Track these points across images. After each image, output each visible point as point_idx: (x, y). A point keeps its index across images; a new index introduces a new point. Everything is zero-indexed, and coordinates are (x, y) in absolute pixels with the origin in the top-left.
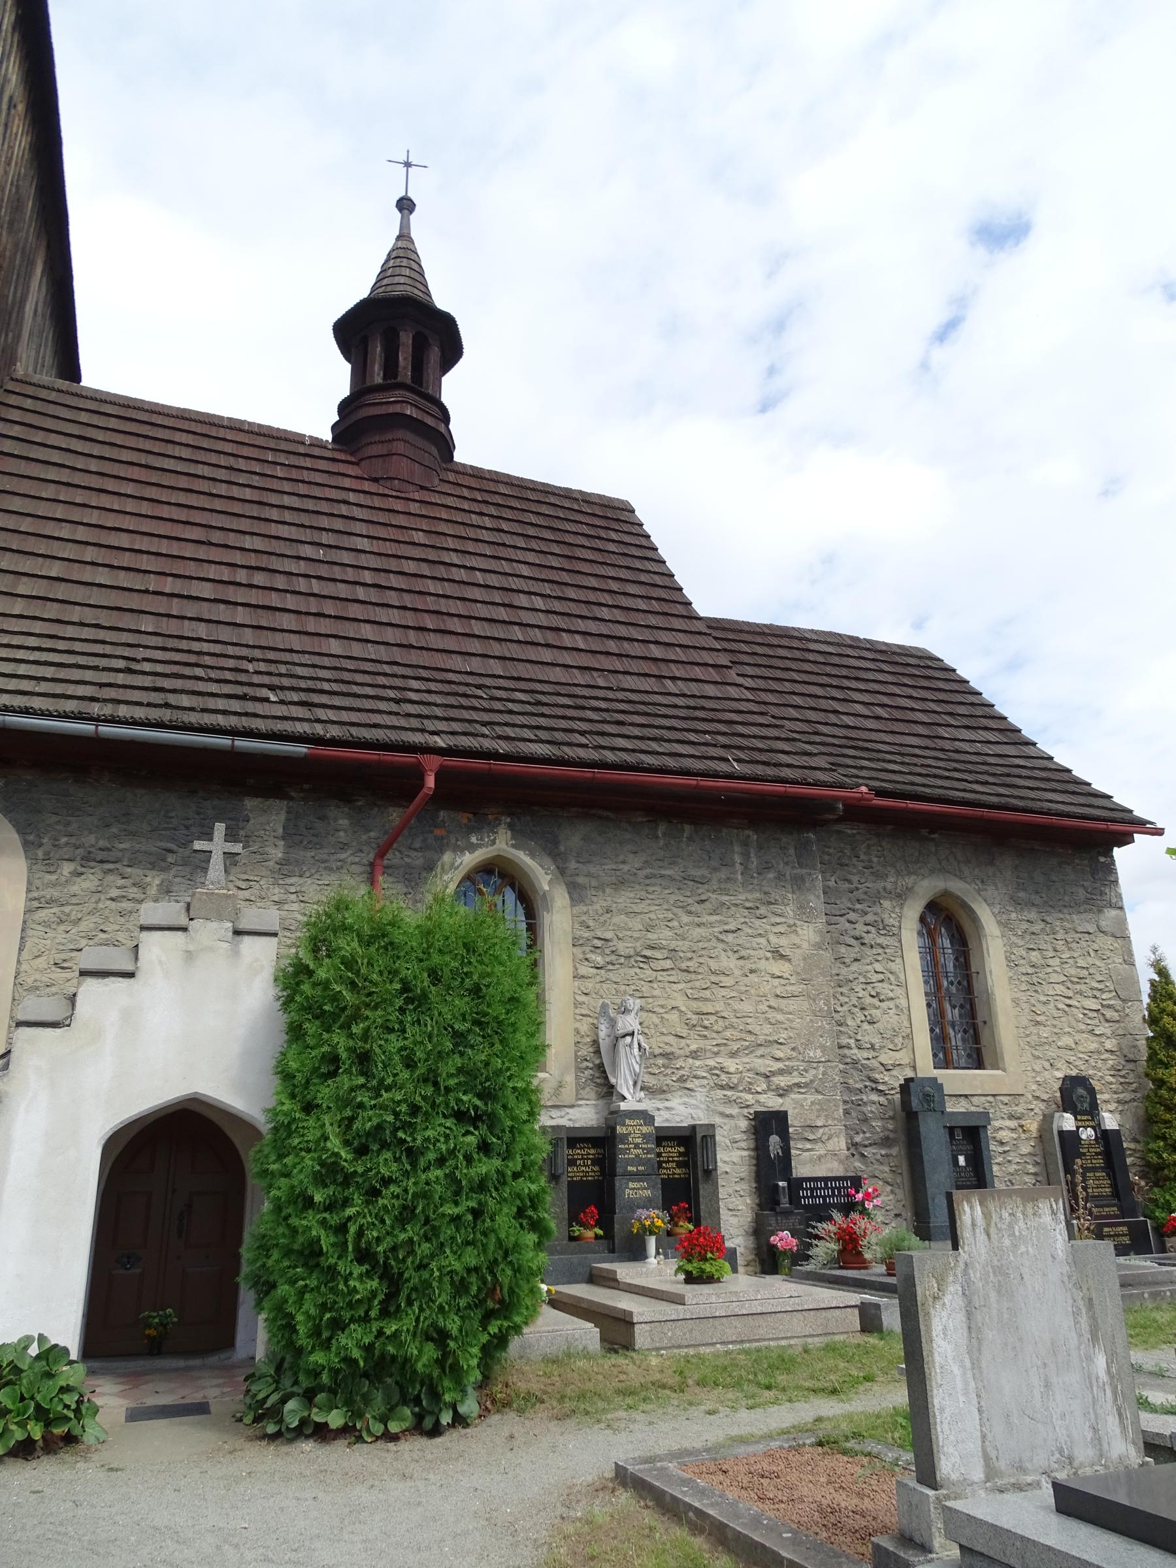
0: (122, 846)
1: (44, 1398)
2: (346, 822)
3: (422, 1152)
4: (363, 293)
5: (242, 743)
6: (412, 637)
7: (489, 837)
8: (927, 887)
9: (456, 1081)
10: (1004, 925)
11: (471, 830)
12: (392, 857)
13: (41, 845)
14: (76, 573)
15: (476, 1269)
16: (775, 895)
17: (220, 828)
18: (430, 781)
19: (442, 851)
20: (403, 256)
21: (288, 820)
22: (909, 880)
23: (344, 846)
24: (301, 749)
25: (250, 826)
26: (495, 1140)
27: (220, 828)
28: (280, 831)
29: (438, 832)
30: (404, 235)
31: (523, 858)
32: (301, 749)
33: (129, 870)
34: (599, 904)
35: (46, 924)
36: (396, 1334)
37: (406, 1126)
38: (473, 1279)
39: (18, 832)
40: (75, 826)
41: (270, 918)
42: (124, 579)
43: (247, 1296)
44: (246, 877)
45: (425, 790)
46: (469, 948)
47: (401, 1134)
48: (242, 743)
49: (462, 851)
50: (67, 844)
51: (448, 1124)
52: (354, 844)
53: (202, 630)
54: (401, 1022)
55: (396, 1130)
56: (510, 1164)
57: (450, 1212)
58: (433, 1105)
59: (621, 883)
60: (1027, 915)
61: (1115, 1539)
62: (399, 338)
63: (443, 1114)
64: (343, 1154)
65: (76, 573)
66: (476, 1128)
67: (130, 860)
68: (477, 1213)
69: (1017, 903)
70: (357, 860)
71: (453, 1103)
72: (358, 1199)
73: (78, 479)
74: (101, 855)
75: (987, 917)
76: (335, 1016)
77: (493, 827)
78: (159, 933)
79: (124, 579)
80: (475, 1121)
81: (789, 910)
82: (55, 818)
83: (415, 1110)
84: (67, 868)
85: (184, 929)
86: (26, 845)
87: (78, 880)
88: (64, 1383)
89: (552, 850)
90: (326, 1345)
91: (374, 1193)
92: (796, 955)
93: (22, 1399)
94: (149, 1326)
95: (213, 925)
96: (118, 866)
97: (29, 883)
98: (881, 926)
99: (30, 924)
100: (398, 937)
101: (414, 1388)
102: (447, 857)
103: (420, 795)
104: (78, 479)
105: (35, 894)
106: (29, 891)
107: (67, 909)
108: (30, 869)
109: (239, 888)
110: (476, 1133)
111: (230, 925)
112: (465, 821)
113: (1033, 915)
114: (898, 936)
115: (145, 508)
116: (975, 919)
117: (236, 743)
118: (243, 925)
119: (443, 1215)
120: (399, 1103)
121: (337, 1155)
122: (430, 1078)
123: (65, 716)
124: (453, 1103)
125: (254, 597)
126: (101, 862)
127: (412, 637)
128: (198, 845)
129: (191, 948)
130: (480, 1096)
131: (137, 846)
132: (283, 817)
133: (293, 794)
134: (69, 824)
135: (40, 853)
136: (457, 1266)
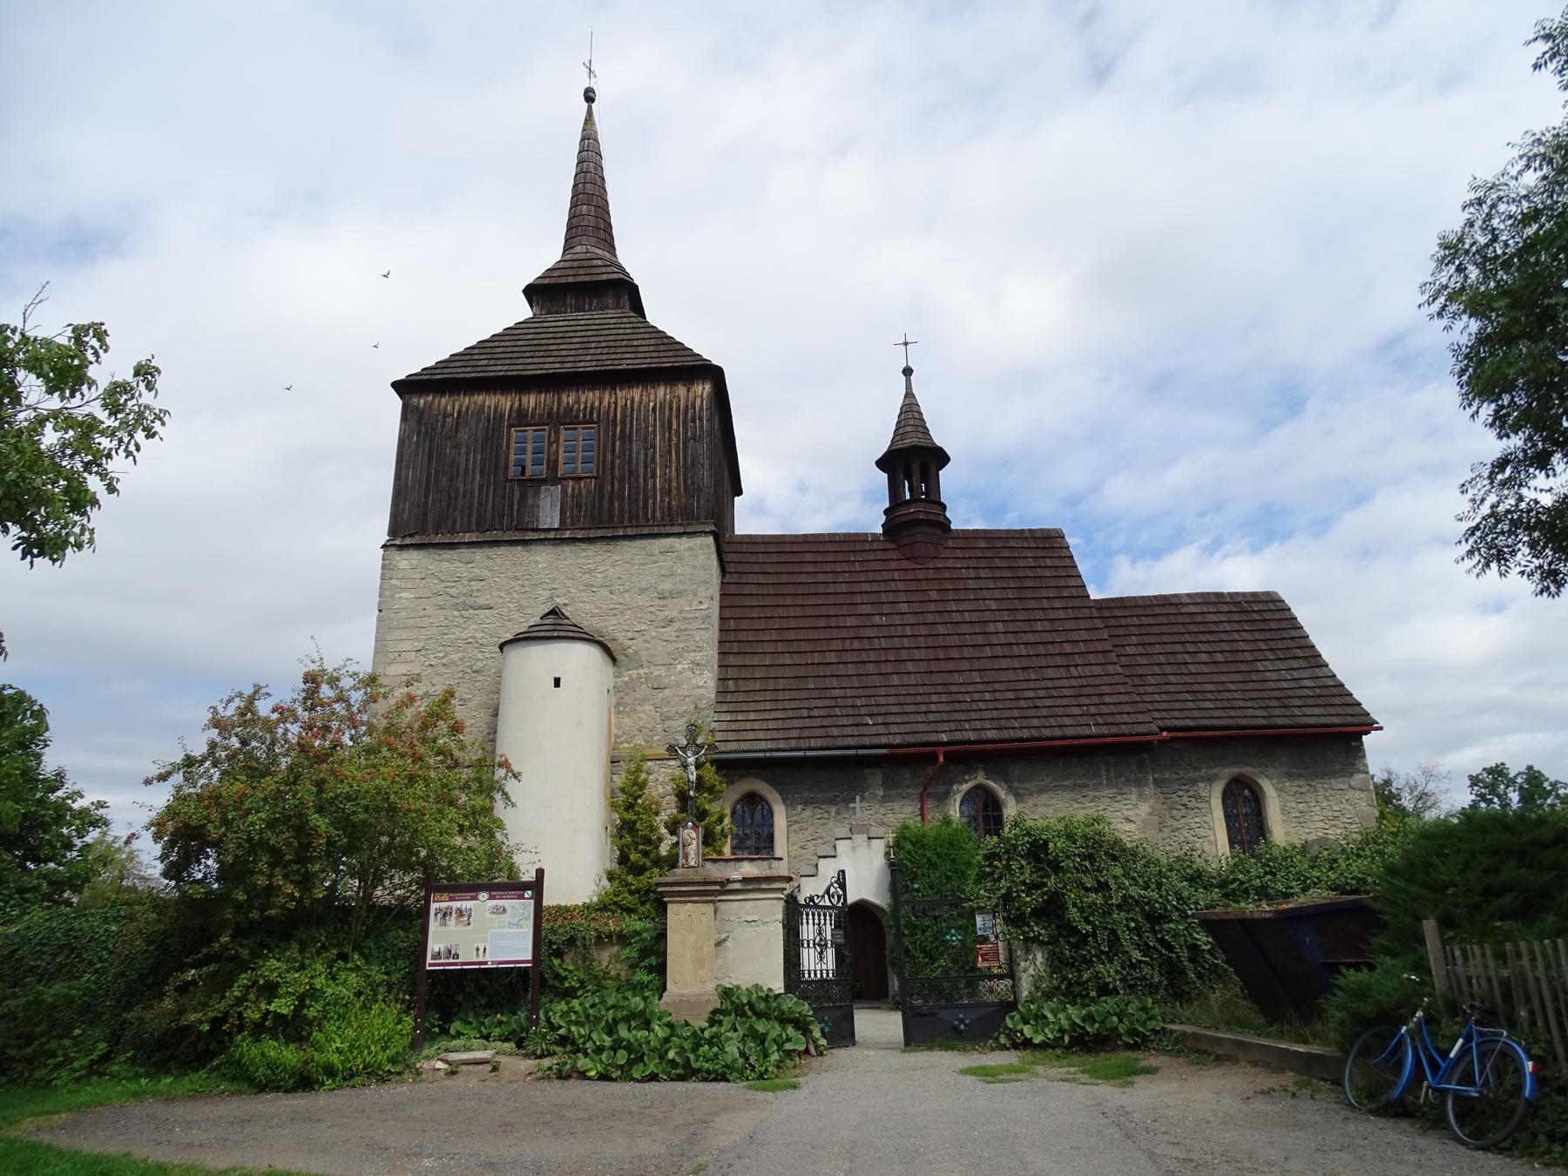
4: (885, 450)
5: (861, 752)
6: (933, 666)
8: (1228, 772)
10: (1280, 790)
11: (965, 773)
12: (931, 790)
16: (1125, 790)
18: (941, 759)
20: (910, 413)
22: (1216, 771)
24: (885, 751)
30: (909, 394)
31: (992, 784)
32: (885, 751)
34: (1031, 802)
41: (881, 831)
43: (889, 969)
46: (951, 844)
48: (861, 752)
59: (1041, 791)
60: (1297, 782)
61: (1391, 1136)
62: (913, 461)
69: (1290, 776)
75: (1269, 788)
77: (975, 771)
81: (1133, 797)
86: (784, 800)
89: (1004, 778)
91: (924, 932)
92: (1138, 820)
98: (1198, 797)
100: (925, 841)
113: (1301, 783)
114: (1208, 802)
116: (1261, 788)
123: (792, 750)
127: (933, 666)
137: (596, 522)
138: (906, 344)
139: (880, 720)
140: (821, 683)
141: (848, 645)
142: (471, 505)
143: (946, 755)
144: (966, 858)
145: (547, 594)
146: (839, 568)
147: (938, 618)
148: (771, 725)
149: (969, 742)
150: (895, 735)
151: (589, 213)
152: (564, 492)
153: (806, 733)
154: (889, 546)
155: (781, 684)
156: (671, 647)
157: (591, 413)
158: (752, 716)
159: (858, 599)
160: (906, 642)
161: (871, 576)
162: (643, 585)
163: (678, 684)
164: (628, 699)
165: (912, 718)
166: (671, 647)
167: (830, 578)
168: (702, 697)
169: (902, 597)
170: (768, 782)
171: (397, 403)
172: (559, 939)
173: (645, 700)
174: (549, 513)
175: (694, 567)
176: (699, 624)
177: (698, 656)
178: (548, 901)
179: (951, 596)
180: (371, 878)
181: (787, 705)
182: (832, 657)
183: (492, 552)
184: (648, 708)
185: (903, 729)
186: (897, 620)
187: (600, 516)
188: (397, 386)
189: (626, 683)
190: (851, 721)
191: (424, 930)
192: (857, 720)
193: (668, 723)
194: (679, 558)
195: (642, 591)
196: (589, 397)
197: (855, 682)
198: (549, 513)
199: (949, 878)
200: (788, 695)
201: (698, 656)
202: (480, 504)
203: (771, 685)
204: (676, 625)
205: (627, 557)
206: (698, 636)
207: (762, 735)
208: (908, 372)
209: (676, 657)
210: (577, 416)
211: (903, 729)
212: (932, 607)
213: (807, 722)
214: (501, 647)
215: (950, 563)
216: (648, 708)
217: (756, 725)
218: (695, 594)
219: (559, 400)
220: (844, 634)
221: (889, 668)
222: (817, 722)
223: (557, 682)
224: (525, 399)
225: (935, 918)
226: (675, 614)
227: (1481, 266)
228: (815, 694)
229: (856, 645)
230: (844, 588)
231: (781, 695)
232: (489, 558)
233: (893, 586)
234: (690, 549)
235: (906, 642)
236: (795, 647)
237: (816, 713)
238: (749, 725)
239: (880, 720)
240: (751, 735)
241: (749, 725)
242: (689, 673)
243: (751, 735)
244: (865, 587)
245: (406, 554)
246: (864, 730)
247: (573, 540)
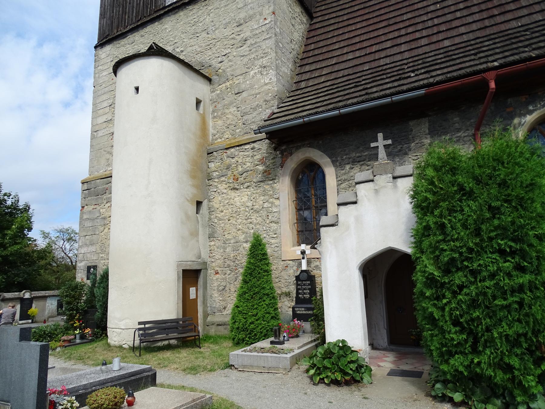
0: (365, 154)
1: (342, 365)
2: (458, 119)
3: (480, 272)
5: (395, 98)
7: (540, 104)
9: (495, 233)
11: (528, 103)
13: (337, 161)
14: (341, 59)
15: (525, 335)
17: (380, 136)
18: (493, 85)
19: (512, 118)
21: (429, 125)
23: (459, 130)
24: (422, 92)
25: (413, 133)
26: (526, 264)
27: (380, 136)
28: (427, 131)
29: (508, 110)
32: (422, 92)
33: (369, 162)
35: (345, 189)
36: (479, 363)
37: (467, 259)
38: (522, 339)
39: (330, 158)
40: (347, 151)
42: (358, 54)
44: (416, 154)
45: (490, 90)
47: (466, 263)
48: (395, 98)
49: (525, 115)
50: (346, 158)
51: (494, 257)
52: (464, 128)
53: (388, 60)
54: (461, 206)
55: (462, 261)
56: (539, 278)
57: (500, 303)
58: (482, 248)
63: (490, 251)
64: (436, 273)
65: (341, 59)
66: (513, 258)
67: (369, 158)
68: (521, 304)
70: (466, 134)
71: (495, 246)
72: (448, 295)
73: (340, 25)
74: (358, 159)
76: (427, 207)
78: (363, 184)
79: (358, 54)
80: (513, 253)
82: (340, 150)
83: (470, 250)
84: (348, 167)
85: (372, 181)
86: (334, 163)
87: (352, 170)
88: (349, 360)
90: (447, 362)
93: (333, 364)
94: (412, 335)
95: (384, 177)
96: (365, 162)
97: (337, 175)
99: (340, 190)
101: (499, 390)
102: (516, 121)
103: (489, 93)
104: (340, 25)
105: (339, 179)
106: (337, 178)
107: (351, 182)
108: (336, 170)
109: (414, 160)
110: (513, 261)
111: (391, 175)
112: (524, 100)
115: (364, 24)
117: (393, 99)
118: (397, 174)
119: (497, 305)
120: (461, 247)
121: (432, 274)
122: (477, 232)
123: (329, 110)
124: (495, 246)
125: (408, 38)
126: (359, 162)
128: (373, 145)
129: (377, 188)
130: (513, 240)
131: (370, 153)
132: (427, 125)
133: (430, 114)
134: (345, 151)
135: (338, 164)
136: (510, 332)
142: (133, 7)
144: (526, 177)
149: (531, 59)
156: (246, 59)
162: (227, 20)
163: (252, 87)
164: (219, 106)
170: (319, 149)
173: (231, 103)
176: (265, 36)
177: (265, 61)
183: (142, 32)
184: (233, 109)
189: (218, 95)
199: (495, 211)
201: (265, 61)
202: (137, 4)
204: (248, 42)
206: (264, 45)
209: (248, 67)
214: (339, 205)
216: (233, 109)
218: (261, 14)
225: (474, 273)
226: (248, 34)
227: (475, 308)
232: (142, 36)
242: (259, 76)
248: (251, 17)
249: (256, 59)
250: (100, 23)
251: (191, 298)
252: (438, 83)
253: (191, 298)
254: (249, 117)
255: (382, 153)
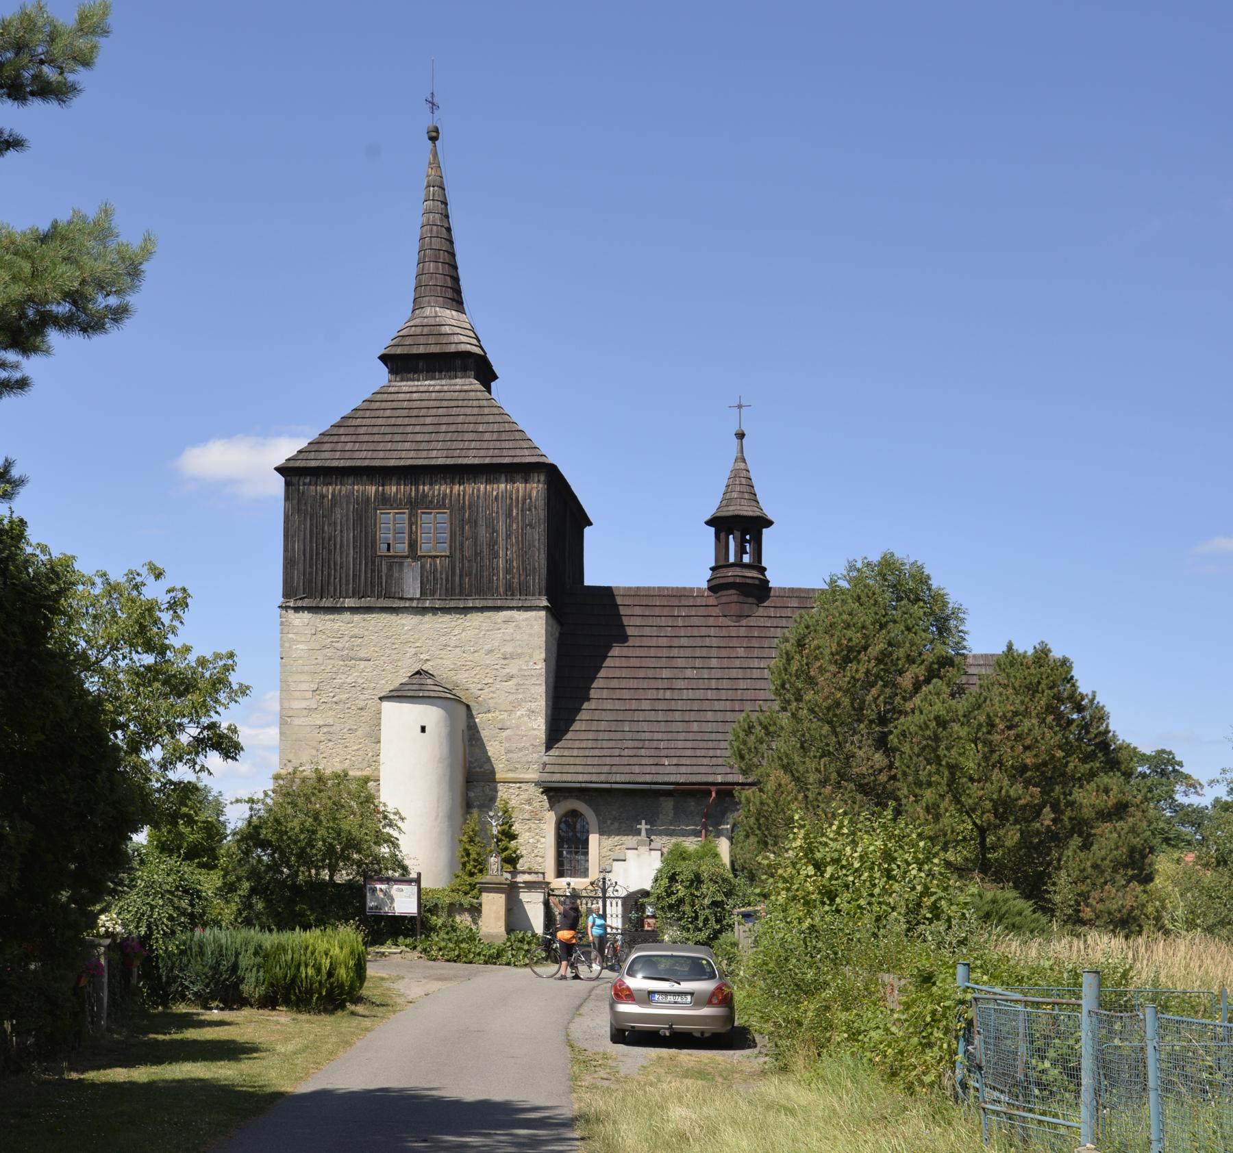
18: (714, 794)
20: (742, 482)
24: (672, 787)
32: (672, 787)
48: (653, 786)
137: (450, 593)
138: (740, 407)
139: (675, 761)
140: (635, 727)
141: (661, 694)
143: (718, 792)
145: (413, 651)
146: (663, 622)
147: (740, 674)
148: (590, 761)
150: (682, 775)
151: (444, 280)
152: (423, 567)
153: (614, 769)
154: (712, 601)
155: (603, 726)
156: (512, 697)
157: (444, 499)
158: (575, 753)
159: (675, 652)
160: (710, 694)
161: (690, 632)
165: (700, 761)
166: (512, 697)
167: (655, 632)
168: (535, 737)
169: (714, 653)
171: (281, 480)
172: (429, 905)
174: (411, 586)
175: (530, 635)
177: (533, 706)
178: (423, 885)
179: (756, 653)
180: (333, 870)
181: (605, 744)
182: (646, 705)
185: (689, 769)
186: (705, 673)
187: (453, 588)
188: (280, 470)
190: (651, 761)
191: (365, 897)
192: (656, 760)
193: (510, 755)
194: (518, 627)
195: (490, 652)
196: (442, 489)
197: (663, 727)
198: (411, 586)
200: (606, 736)
201: (533, 706)
203: (594, 726)
205: (476, 624)
207: (580, 769)
208: (741, 436)
209: (516, 705)
210: (431, 502)
211: (689, 769)
212: (737, 663)
213: (617, 760)
214: (380, 699)
215: (762, 622)
217: (578, 761)
218: (531, 657)
219: (417, 491)
220: (660, 684)
221: (693, 716)
222: (625, 761)
223: (423, 729)
224: (387, 488)
226: (514, 672)
228: (629, 736)
229: (668, 694)
230: (664, 642)
231: (601, 736)
233: (707, 642)
234: (527, 619)
235: (710, 694)
236: (618, 694)
237: (626, 752)
238: (572, 761)
239: (675, 761)
240: (572, 769)
241: (572, 761)
242: (526, 719)
243: (572, 769)
244: (684, 642)
245: (301, 614)
246: (660, 769)
247: (434, 610)
248: (519, 655)
249: (524, 700)
250: (286, 550)
251: (586, 583)
252: (682, 784)
253: (586, 583)
254: (515, 756)
255: (643, 833)
